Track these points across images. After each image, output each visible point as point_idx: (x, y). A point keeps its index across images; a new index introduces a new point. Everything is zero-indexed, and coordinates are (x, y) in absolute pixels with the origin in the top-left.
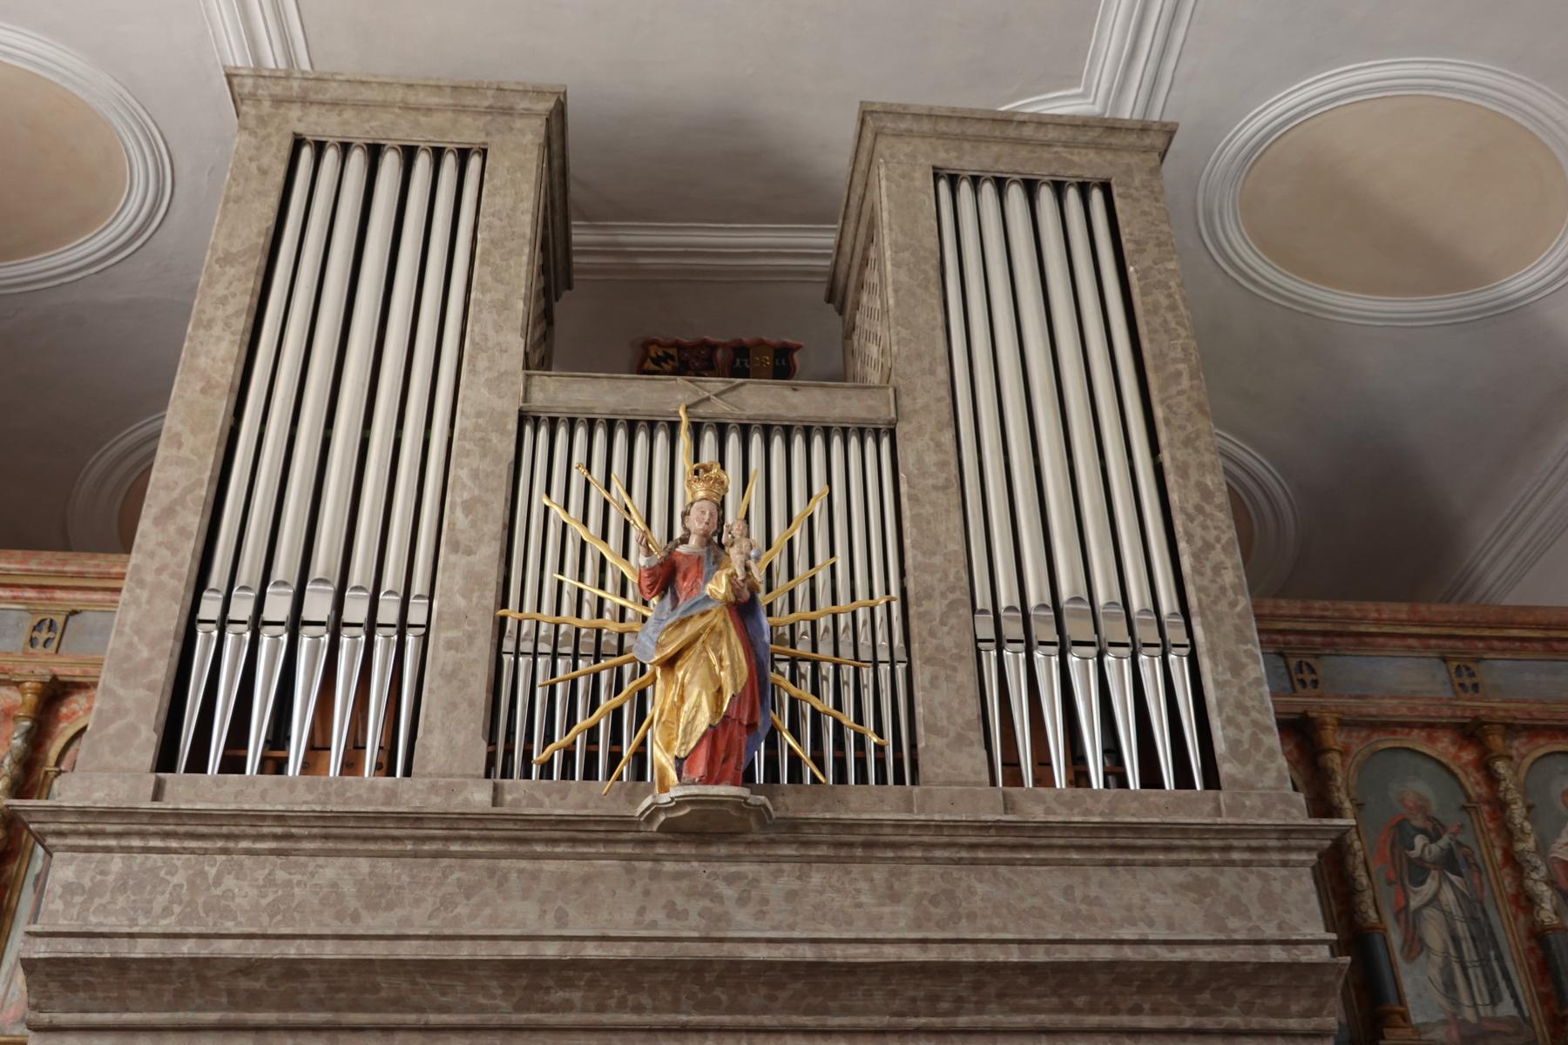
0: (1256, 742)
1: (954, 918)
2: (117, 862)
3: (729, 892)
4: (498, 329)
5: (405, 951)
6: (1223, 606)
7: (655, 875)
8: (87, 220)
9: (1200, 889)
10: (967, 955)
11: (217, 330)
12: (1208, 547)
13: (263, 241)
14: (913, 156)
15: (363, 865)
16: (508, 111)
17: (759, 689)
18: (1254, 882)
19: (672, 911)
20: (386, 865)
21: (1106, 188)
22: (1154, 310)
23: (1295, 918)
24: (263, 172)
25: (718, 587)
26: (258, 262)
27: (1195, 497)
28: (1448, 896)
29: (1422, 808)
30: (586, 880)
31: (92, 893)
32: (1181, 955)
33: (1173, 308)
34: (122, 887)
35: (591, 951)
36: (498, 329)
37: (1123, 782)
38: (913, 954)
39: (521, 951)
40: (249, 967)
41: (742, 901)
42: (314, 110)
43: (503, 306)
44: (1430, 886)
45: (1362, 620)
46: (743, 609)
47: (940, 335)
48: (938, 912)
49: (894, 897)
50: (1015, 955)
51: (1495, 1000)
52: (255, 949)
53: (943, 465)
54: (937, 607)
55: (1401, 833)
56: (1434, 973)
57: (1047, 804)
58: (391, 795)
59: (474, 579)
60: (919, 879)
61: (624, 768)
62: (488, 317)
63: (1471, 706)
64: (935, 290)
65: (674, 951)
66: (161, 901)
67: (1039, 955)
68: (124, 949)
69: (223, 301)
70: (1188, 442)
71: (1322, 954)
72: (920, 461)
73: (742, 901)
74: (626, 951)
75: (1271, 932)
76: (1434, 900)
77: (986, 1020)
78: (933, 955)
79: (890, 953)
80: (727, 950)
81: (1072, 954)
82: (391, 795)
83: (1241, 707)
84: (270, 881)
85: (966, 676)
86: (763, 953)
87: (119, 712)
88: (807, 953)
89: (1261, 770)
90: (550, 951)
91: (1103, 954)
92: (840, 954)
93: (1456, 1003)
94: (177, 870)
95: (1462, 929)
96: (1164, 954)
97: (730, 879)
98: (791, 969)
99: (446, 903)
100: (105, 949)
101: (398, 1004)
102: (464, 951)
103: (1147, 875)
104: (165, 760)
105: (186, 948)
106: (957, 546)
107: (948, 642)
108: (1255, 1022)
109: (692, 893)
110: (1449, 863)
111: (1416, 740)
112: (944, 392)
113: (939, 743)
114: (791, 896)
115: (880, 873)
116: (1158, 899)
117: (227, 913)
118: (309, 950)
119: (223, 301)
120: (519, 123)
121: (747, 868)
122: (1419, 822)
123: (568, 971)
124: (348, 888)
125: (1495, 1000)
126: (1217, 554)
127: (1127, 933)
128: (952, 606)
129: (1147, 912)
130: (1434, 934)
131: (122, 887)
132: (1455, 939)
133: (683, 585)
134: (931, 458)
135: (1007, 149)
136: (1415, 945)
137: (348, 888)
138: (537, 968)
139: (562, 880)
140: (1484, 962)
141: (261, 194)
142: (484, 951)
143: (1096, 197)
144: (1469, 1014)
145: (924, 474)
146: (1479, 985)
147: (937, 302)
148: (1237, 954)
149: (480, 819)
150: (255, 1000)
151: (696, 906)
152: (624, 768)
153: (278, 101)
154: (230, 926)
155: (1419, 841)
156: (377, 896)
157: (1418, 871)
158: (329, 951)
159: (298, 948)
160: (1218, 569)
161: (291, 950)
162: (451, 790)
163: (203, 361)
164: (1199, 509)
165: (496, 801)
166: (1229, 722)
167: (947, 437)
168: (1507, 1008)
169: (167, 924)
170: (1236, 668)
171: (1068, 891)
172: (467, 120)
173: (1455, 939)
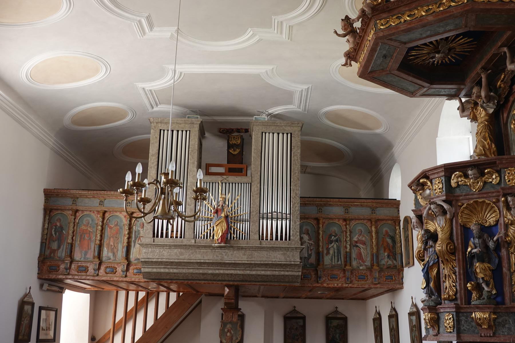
0: (296, 233)
1: (252, 258)
2: (150, 249)
3: (224, 254)
4: (193, 167)
5: (185, 261)
6: (295, 213)
7: (215, 252)
8: (124, 118)
9: (284, 254)
10: (253, 262)
11: (153, 169)
12: (295, 203)
13: (157, 151)
14: (259, 130)
15: (179, 250)
16: (193, 123)
17: (229, 228)
18: (292, 253)
19: (217, 256)
20: (182, 250)
21: (291, 134)
22: (294, 160)
23: (296, 258)
24: (156, 138)
25: (223, 215)
26: (157, 156)
27: (294, 195)
28: (335, 246)
29: (335, 232)
30: (206, 252)
31: (148, 253)
32: (280, 263)
33: (297, 160)
34: (151, 253)
35: (207, 261)
36: (193, 167)
37: (278, 240)
38: (246, 262)
39: (199, 261)
40: (167, 262)
41: (226, 255)
42: (163, 124)
43: (194, 163)
44: (333, 244)
45: (330, 202)
46: (227, 217)
47: (260, 166)
48: (250, 257)
49: (245, 255)
50: (259, 262)
51: (338, 261)
52: (167, 260)
53: (257, 190)
54: (254, 213)
55: (330, 236)
56: (330, 257)
57: (264, 244)
58: (182, 242)
59: (191, 210)
60: (248, 252)
61: (211, 238)
62: (191, 165)
63: (347, 216)
64: (260, 158)
65: (217, 261)
66: (156, 254)
67: (262, 262)
68: (152, 260)
69: (153, 163)
70: (295, 185)
71: (299, 263)
72: (254, 190)
73: (226, 255)
74: (211, 261)
75: (293, 260)
76: (333, 246)
77: (256, 269)
78: (249, 262)
79: (244, 262)
80: (223, 261)
81: (266, 262)
82: (182, 242)
83: (295, 229)
84: (168, 252)
85: (257, 224)
86: (228, 262)
87: (148, 229)
88: (233, 262)
89: (296, 238)
90: (202, 261)
91: (270, 262)
92: (237, 262)
93: (332, 262)
94: (157, 250)
95: (336, 251)
96: (278, 263)
97: (224, 252)
98: (231, 263)
99: (190, 255)
100: (150, 260)
101: (184, 266)
102: (192, 261)
103: (278, 252)
104: (154, 236)
105: (160, 260)
106: (258, 204)
107: (255, 219)
108: (291, 270)
109: (219, 254)
110: (337, 241)
111: (336, 221)
112: (259, 177)
113: (253, 234)
114: (232, 255)
115: (243, 252)
116: (279, 256)
117: (164, 256)
118: (174, 260)
119: (153, 163)
120: (195, 126)
121: (226, 251)
122: (333, 234)
123: (204, 263)
124: (178, 253)
125: (338, 261)
126: (296, 205)
127: (274, 260)
128: (256, 213)
129: (278, 257)
130: (331, 252)
131: (151, 253)
132: (334, 252)
133: (219, 213)
134: (256, 189)
135: (275, 127)
136: (328, 253)
137: (178, 253)
138: (201, 263)
139: (204, 252)
140: (338, 256)
141: (156, 142)
142: (194, 261)
143: (289, 135)
144: (334, 263)
145: (254, 192)
146: (336, 258)
147: (260, 160)
148: (288, 263)
149: (193, 245)
150: (167, 265)
151: (220, 256)
152: (211, 238)
153: (157, 123)
154: (164, 257)
155: (333, 237)
156: (181, 254)
157: (331, 242)
158: (176, 261)
159: (152, 155)
160: (295, 207)
161: (172, 261)
162: (190, 241)
163: (151, 174)
164: (295, 197)
165: (195, 242)
166: (293, 231)
167: (259, 185)
168: (340, 262)
169: (157, 257)
170: (295, 223)
171: (267, 254)
172: (187, 125)
173: (334, 252)
